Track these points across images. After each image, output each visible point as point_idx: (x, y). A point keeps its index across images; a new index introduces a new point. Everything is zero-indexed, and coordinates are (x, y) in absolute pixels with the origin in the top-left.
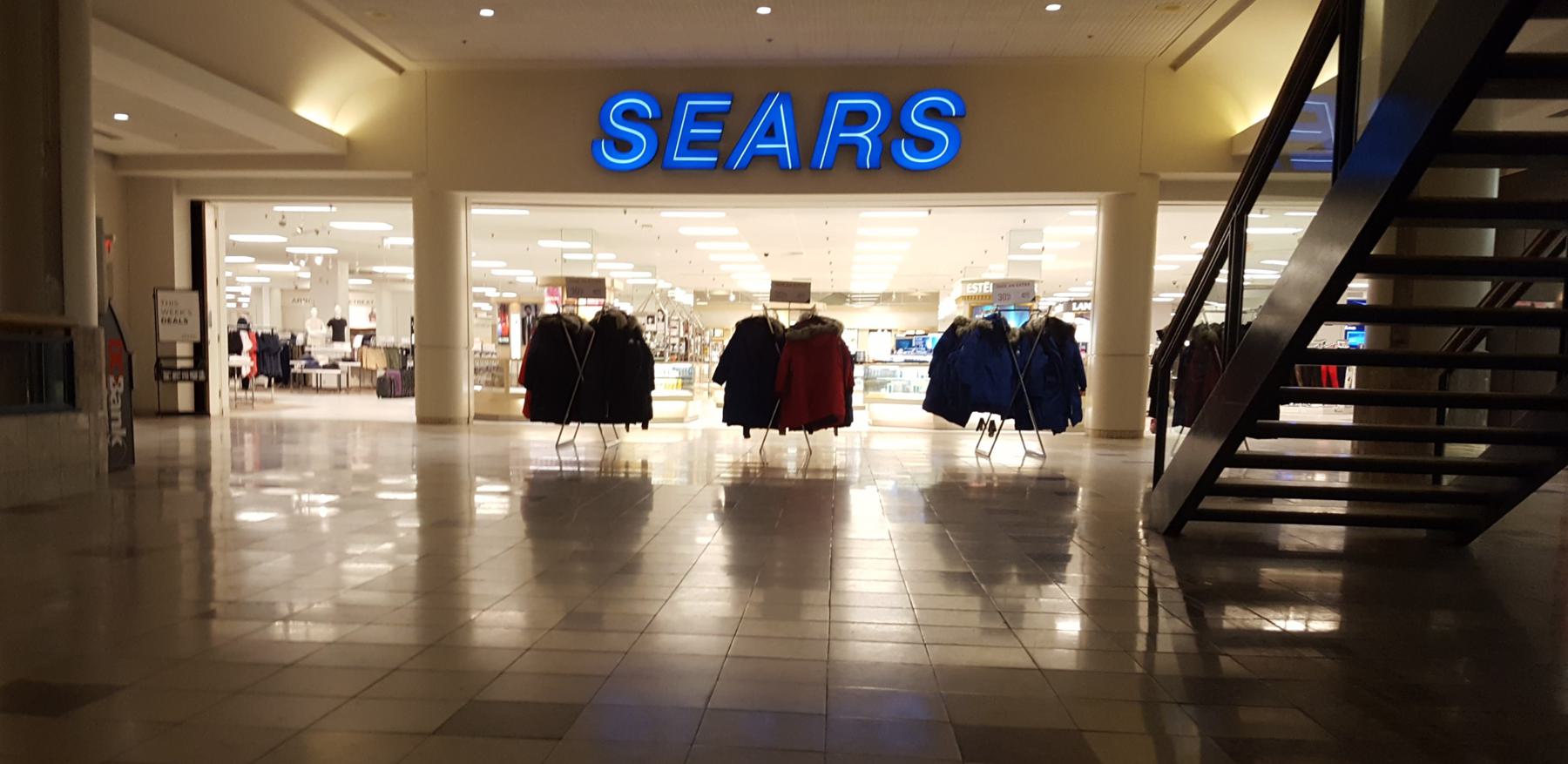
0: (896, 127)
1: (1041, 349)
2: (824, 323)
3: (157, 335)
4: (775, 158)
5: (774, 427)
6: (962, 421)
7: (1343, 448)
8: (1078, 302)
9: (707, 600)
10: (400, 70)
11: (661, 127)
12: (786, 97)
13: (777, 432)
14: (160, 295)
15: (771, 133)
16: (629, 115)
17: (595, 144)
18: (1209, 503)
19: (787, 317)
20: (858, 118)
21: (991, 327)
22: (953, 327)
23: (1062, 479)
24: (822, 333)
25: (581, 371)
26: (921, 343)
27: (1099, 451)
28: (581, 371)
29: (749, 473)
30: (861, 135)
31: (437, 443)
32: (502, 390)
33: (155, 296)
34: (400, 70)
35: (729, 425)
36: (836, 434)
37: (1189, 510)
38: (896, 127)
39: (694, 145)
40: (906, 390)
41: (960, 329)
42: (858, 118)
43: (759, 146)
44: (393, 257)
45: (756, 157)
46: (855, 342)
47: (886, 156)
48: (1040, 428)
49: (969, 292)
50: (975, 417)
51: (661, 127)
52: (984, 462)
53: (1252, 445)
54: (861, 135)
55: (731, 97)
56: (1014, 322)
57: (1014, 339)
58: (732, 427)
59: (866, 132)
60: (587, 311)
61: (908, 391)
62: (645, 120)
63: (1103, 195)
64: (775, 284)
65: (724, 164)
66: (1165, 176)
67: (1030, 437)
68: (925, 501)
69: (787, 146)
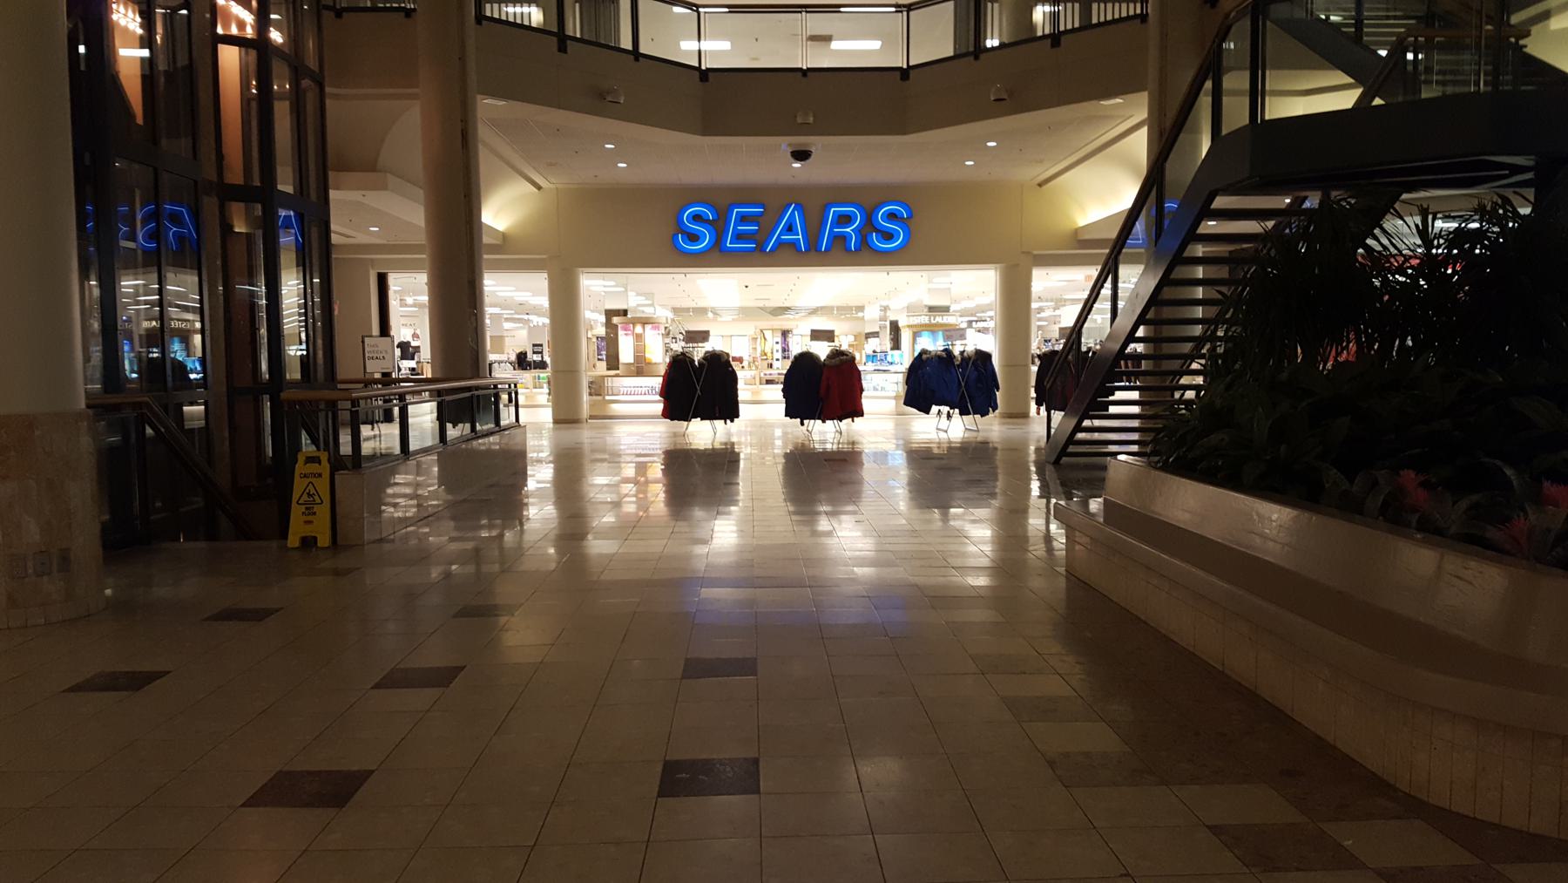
0: (869, 223)
2: (847, 355)
4: (794, 245)
5: (819, 419)
6: (927, 411)
7: (1135, 423)
9: (1158, 401)
10: (539, 188)
12: (799, 206)
13: (820, 421)
14: (366, 339)
15: (790, 229)
16: (697, 218)
17: (675, 235)
18: (1071, 449)
19: (822, 350)
21: (945, 356)
22: (920, 354)
23: (988, 443)
24: (843, 363)
26: (883, 358)
27: (1004, 424)
29: (1210, 412)
30: (848, 230)
32: (599, 398)
33: (363, 342)
34: (539, 188)
37: (1063, 452)
38: (869, 223)
39: (739, 237)
42: (845, 219)
43: (783, 237)
44: (535, 310)
48: (974, 414)
49: (911, 323)
50: (935, 409)
53: (1086, 423)
54: (848, 230)
55: (762, 206)
56: (956, 351)
57: (958, 363)
58: (704, 421)
59: (853, 227)
61: (877, 390)
62: (707, 221)
63: (998, 265)
64: (813, 331)
65: (761, 248)
66: (1035, 252)
67: (968, 419)
68: (993, 443)
69: (800, 237)
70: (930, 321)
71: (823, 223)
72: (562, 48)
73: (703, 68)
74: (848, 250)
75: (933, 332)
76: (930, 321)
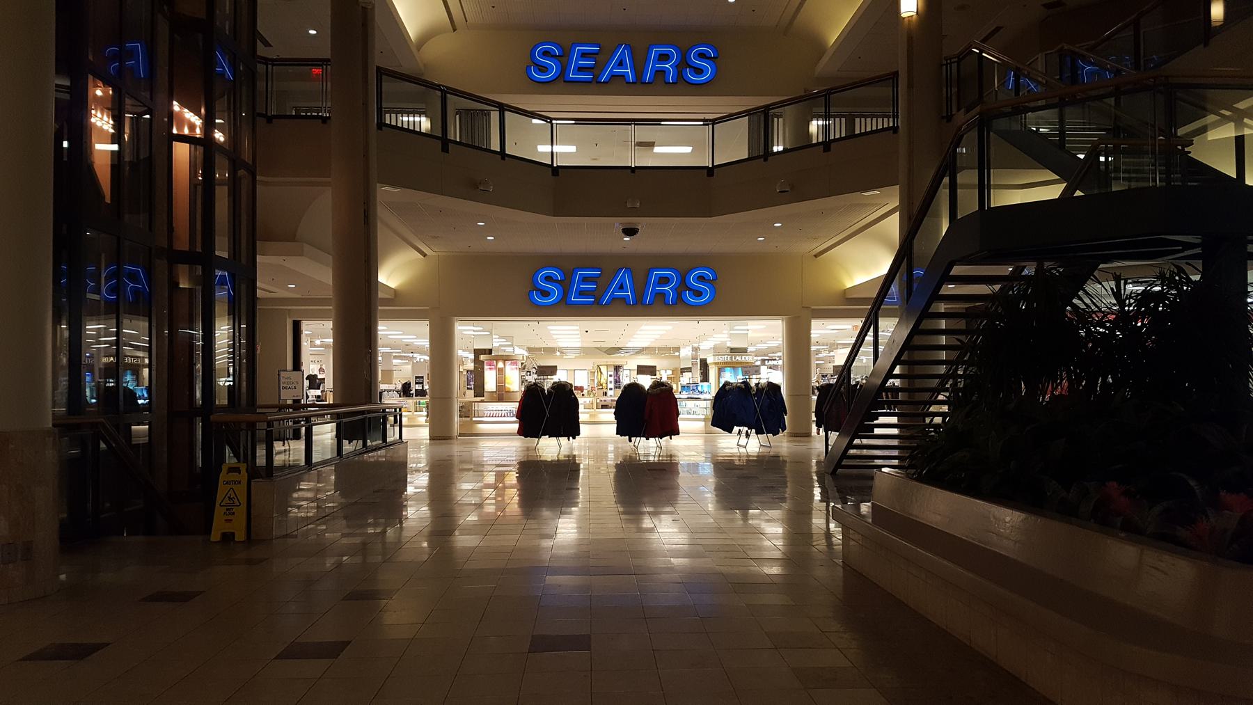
0: (683, 285)
1: (766, 397)
2: (666, 386)
3: (280, 396)
4: (624, 300)
8: (768, 360)
10: (425, 255)
11: (565, 285)
12: (629, 270)
16: (548, 279)
18: (845, 462)
19: (646, 382)
20: (664, 280)
24: (666, 390)
25: (547, 412)
28: (547, 412)
31: (442, 449)
32: (468, 419)
33: (279, 375)
34: (425, 255)
35: (579, 434)
36: (671, 438)
37: (839, 465)
39: (582, 293)
40: (689, 413)
41: (727, 387)
42: (664, 280)
44: (419, 350)
45: (614, 299)
46: (628, 378)
47: (679, 298)
49: (717, 361)
50: (736, 429)
51: (565, 285)
52: (742, 450)
53: (857, 442)
56: (753, 383)
60: (547, 384)
65: (598, 302)
66: (813, 307)
70: (732, 359)
71: (647, 59)
72: (445, 149)
73: (555, 165)
74: (667, 304)
75: (734, 368)
76: (732, 359)
